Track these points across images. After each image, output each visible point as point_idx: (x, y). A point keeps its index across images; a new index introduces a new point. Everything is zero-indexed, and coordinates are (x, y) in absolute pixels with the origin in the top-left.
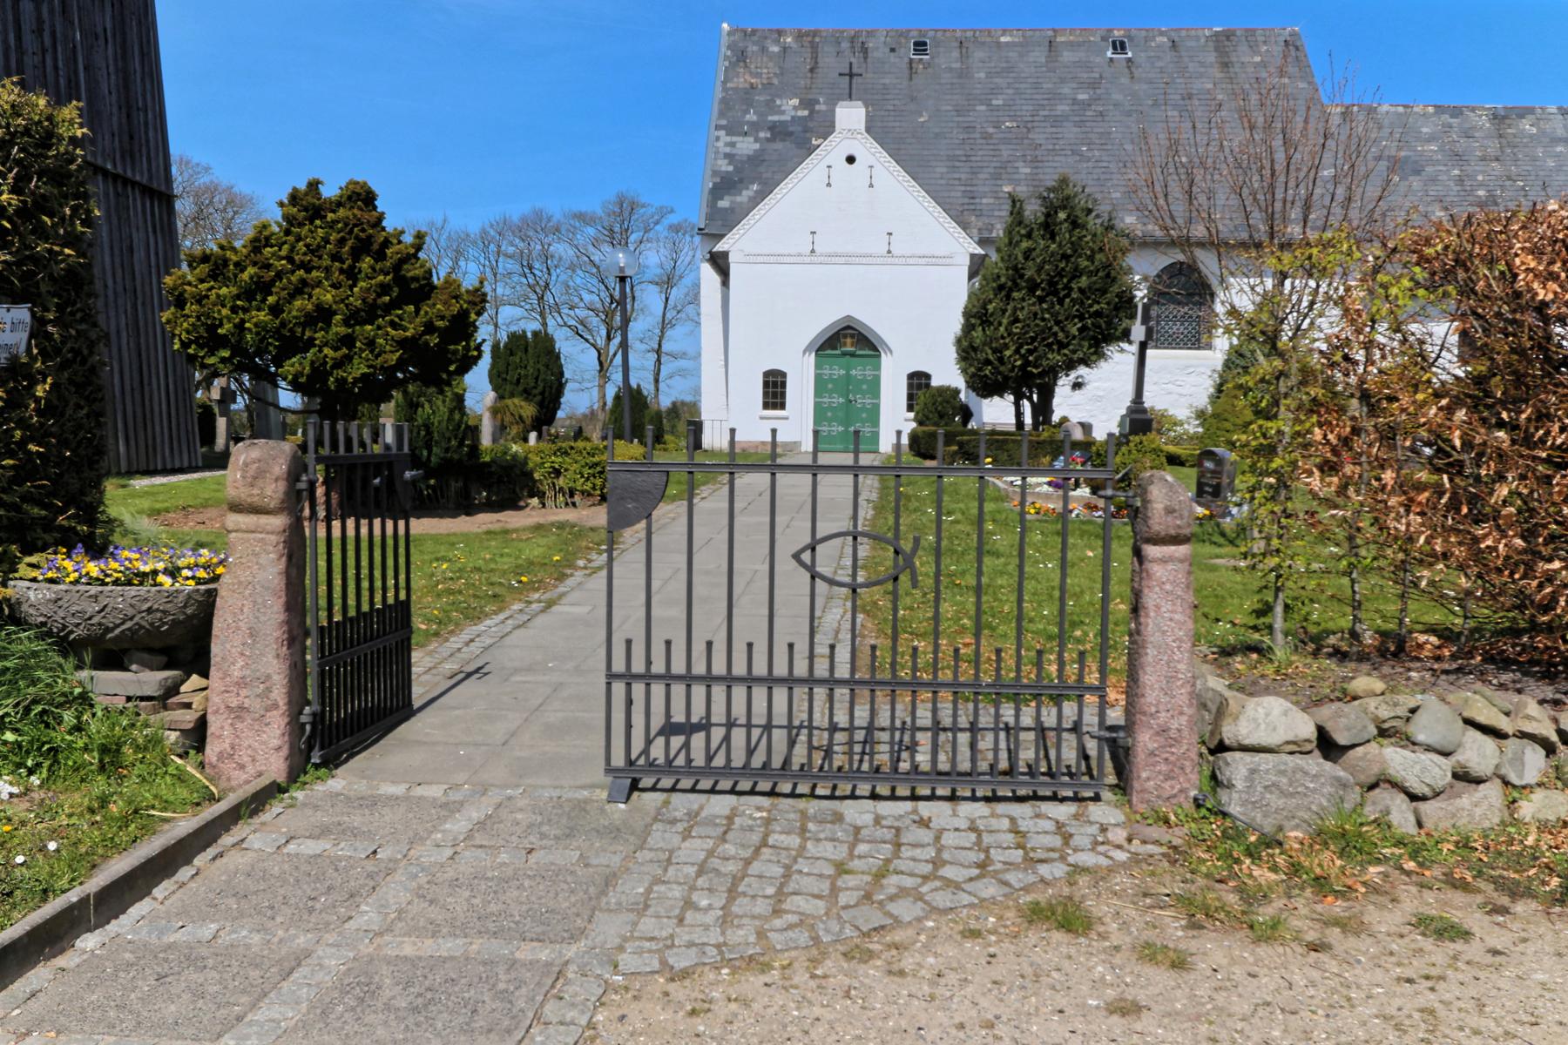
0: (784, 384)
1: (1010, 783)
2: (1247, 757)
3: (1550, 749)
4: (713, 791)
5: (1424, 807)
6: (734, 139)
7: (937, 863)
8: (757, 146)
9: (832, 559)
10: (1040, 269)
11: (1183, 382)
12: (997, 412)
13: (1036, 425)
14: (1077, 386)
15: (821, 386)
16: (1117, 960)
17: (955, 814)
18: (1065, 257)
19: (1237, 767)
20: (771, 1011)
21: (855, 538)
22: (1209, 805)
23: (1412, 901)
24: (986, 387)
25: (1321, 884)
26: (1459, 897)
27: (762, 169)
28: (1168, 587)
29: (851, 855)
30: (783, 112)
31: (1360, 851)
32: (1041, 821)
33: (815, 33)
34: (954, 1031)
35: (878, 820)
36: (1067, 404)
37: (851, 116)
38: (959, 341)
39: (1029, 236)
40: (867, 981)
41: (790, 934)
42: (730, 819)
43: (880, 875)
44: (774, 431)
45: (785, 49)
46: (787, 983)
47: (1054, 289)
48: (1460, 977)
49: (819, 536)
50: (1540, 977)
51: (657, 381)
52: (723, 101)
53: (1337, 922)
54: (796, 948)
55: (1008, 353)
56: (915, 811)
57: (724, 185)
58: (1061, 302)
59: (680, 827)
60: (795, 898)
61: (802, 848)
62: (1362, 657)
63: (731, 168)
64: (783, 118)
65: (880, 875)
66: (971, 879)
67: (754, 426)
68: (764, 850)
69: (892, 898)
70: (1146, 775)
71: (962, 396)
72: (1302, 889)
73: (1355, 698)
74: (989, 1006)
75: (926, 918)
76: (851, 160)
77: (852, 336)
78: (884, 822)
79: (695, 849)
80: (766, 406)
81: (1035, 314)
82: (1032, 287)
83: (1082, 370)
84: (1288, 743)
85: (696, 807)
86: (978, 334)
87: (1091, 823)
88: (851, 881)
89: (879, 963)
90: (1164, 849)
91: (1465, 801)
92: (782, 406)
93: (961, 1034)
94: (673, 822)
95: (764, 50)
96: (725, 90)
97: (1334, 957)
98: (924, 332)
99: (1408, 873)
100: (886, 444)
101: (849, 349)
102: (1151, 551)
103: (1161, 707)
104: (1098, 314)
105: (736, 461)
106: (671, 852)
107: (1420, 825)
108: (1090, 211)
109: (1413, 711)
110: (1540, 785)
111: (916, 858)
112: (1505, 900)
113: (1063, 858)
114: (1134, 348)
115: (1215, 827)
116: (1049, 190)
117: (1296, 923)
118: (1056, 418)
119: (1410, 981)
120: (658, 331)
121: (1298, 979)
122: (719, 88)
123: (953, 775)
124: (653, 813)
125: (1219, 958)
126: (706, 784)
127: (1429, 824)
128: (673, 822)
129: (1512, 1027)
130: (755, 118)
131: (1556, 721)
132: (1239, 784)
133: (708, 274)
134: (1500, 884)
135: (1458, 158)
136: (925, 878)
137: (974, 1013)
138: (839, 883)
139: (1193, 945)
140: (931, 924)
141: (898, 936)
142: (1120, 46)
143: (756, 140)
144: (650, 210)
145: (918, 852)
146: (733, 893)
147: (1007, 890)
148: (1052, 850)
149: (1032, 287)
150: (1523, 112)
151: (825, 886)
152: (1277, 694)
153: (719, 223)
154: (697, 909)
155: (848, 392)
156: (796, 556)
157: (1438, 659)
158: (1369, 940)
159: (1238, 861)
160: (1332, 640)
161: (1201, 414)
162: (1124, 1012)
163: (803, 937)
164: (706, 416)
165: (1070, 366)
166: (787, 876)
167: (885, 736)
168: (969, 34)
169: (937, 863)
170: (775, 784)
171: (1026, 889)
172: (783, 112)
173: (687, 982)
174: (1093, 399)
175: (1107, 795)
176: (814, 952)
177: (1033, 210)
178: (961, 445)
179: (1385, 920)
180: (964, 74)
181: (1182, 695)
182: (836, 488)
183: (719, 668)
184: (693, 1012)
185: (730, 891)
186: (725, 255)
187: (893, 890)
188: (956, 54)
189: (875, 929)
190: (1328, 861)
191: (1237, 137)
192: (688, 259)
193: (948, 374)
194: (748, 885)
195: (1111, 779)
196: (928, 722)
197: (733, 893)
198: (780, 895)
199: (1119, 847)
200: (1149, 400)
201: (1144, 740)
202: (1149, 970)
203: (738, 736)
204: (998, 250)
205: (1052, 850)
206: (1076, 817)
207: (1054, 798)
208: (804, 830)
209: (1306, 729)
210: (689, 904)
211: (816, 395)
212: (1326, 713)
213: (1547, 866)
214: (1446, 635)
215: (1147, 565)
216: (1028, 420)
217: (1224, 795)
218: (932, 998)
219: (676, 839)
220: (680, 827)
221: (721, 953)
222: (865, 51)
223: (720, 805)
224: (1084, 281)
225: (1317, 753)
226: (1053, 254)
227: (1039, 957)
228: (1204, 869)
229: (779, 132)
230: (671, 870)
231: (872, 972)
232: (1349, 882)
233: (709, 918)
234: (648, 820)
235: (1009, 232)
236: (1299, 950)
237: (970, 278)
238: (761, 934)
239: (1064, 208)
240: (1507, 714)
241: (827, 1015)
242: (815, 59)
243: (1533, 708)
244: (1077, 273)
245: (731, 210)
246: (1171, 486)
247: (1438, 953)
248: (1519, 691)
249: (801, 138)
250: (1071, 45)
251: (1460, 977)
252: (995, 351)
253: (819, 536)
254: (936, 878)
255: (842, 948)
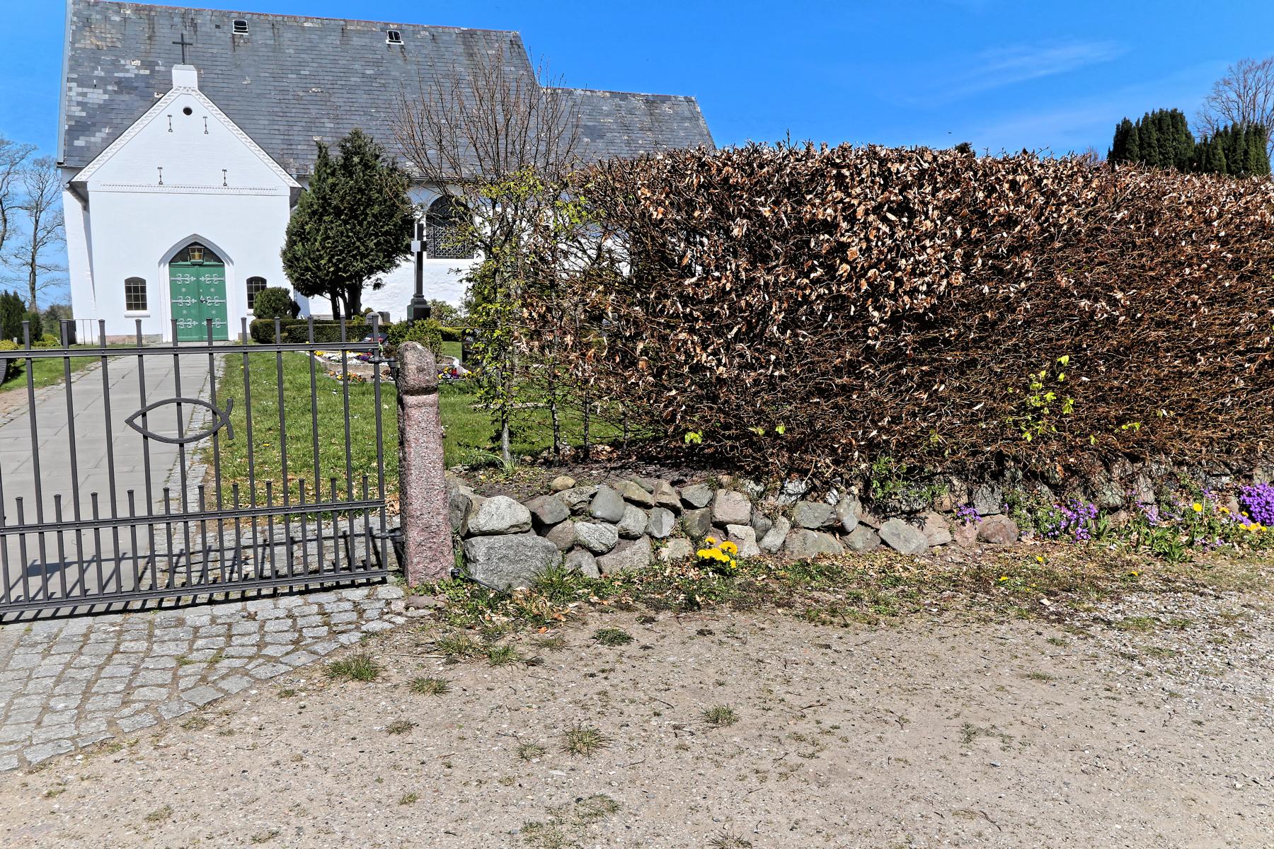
0: (144, 289)
1: (312, 582)
2: (486, 539)
3: (677, 512)
4: (72, 616)
5: (602, 559)
6: (85, 90)
7: (261, 645)
8: (106, 97)
9: (162, 421)
10: (343, 199)
11: (449, 282)
12: (319, 306)
13: (348, 316)
14: (377, 286)
15: (175, 290)
16: (396, 695)
17: (276, 607)
18: (360, 191)
19: (479, 547)
20: (118, 781)
21: (179, 404)
22: (461, 577)
23: (596, 622)
24: (309, 289)
25: (538, 620)
26: (624, 615)
27: (112, 116)
28: (423, 425)
29: (191, 650)
30: (128, 71)
31: (563, 594)
32: (339, 604)
33: (151, 9)
34: (271, 769)
35: (213, 621)
36: (369, 299)
37: (185, 77)
38: (284, 253)
39: (333, 174)
40: (202, 744)
41: (137, 718)
42: (86, 636)
43: (214, 661)
44: (138, 322)
45: (125, 19)
46: (134, 757)
47: (353, 215)
48: (624, 667)
49: (148, 404)
50: (671, 659)
51: (33, 289)
52: (72, 58)
53: (548, 644)
54: (142, 728)
55: (323, 262)
56: (244, 609)
57: (78, 128)
58: (361, 224)
59: (40, 648)
60: (141, 689)
61: (150, 649)
62: (562, 464)
63: (84, 114)
64: (127, 75)
65: (214, 661)
66: (287, 654)
67: (122, 326)
68: (115, 656)
69: (223, 678)
70: (416, 561)
71: (291, 295)
72: (525, 625)
73: (556, 491)
74: (299, 745)
75: (251, 688)
76: (188, 111)
77: (199, 250)
78: (219, 621)
79: (54, 664)
80: (129, 307)
81: (342, 233)
82: (338, 212)
83: (380, 275)
84: (512, 526)
85: (55, 630)
86: (299, 247)
87: (379, 600)
88: (189, 669)
89: (212, 728)
90: (432, 611)
91: (628, 552)
92: (144, 307)
93: (277, 770)
94: (35, 644)
95: (106, 18)
96: (74, 49)
97: (544, 668)
98: (257, 245)
99: (593, 604)
100: (234, 335)
101: (197, 260)
102: (410, 400)
103: (424, 511)
104: (387, 233)
105: (105, 351)
106: (31, 670)
107: (601, 571)
108: (377, 157)
109: (593, 496)
110: (672, 536)
111: (244, 644)
112: (652, 613)
113: (358, 628)
114: (414, 259)
115: (465, 592)
116: (346, 140)
117: (519, 649)
118: (363, 309)
119: (592, 675)
120: (30, 248)
121: (521, 687)
122: (68, 48)
123: (30, 601)
124: (15, 642)
125: (468, 681)
126: (65, 611)
127: (606, 570)
128: (35, 644)
129: (654, 694)
130: (103, 74)
131: (680, 493)
132: (481, 559)
133: (69, 199)
134: (650, 604)
135: (626, 128)
136: (251, 658)
137: (287, 752)
138: (180, 672)
139: (450, 676)
140: (254, 692)
141: (227, 705)
142: (394, 36)
143: (105, 92)
144: (15, 148)
145: (245, 640)
146: (86, 695)
147: (315, 657)
148: (350, 623)
149: (338, 212)
150: (665, 99)
151: (168, 677)
152: (506, 494)
153: (74, 162)
154: (54, 711)
155: (199, 294)
156: (130, 422)
157: (609, 460)
158: (568, 653)
159: (482, 612)
160: (545, 454)
161: (468, 304)
162: (398, 731)
163: (148, 719)
164: (76, 316)
165: (371, 271)
166: (135, 674)
167: (250, 552)
168: (279, 19)
169: (261, 645)
170: (244, 592)
171: (329, 654)
172: (128, 71)
173: (44, 772)
174: (388, 295)
175: (391, 578)
176: (158, 729)
177: (335, 155)
178: (290, 331)
179: (577, 637)
180: (277, 49)
181: (438, 501)
182: (194, 365)
183: (141, 511)
184: (49, 795)
185: (84, 693)
186: (84, 184)
187: (225, 671)
188: (269, 33)
189: (209, 703)
190: (543, 604)
191: (472, 106)
192: (54, 188)
193: (278, 279)
194: (101, 686)
195: (395, 567)
196: (283, 538)
197: (86, 695)
198: (129, 689)
199: (400, 614)
200: (428, 297)
201: (414, 536)
202: (418, 698)
203: (126, 566)
204: (311, 184)
205: (350, 623)
206: (368, 597)
207: (353, 585)
208: (151, 635)
209: (523, 515)
210: (46, 709)
211: (225, 304)
212: (537, 502)
213: (677, 587)
214: (615, 444)
215: (408, 410)
216: (343, 312)
217: (471, 568)
218: (255, 747)
219: (37, 659)
220: (40, 648)
221: (75, 744)
222: (194, 25)
223: (78, 626)
224: (376, 209)
225: (532, 531)
226: (351, 188)
227: (338, 702)
228: (459, 621)
229: (125, 86)
230: (31, 685)
231: (206, 736)
232: (556, 616)
233: (65, 717)
234: (11, 646)
235: (318, 171)
236: (522, 666)
237: (291, 206)
238: (111, 723)
239: (356, 153)
240: (651, 492)
241: (168, 775)
242: (152, 27)
243: (666, 486)
244: (370, 202)
245: (87, 148)
246: (421, 352)
247: (610, 653)
248: (659, 477)
249: (148, 90)
250: (360, 33)
251: (624, 667)
252: (312, 260)
253: (148, 404)
254: (260, 656)
255: (181, 722)
